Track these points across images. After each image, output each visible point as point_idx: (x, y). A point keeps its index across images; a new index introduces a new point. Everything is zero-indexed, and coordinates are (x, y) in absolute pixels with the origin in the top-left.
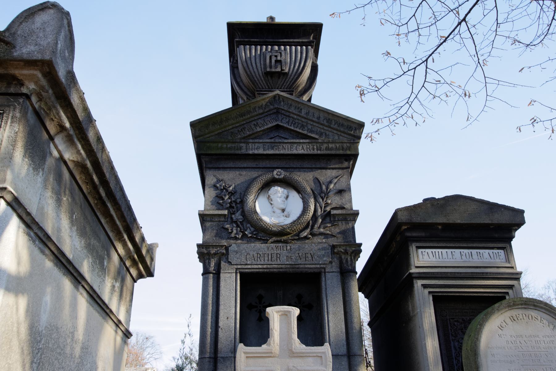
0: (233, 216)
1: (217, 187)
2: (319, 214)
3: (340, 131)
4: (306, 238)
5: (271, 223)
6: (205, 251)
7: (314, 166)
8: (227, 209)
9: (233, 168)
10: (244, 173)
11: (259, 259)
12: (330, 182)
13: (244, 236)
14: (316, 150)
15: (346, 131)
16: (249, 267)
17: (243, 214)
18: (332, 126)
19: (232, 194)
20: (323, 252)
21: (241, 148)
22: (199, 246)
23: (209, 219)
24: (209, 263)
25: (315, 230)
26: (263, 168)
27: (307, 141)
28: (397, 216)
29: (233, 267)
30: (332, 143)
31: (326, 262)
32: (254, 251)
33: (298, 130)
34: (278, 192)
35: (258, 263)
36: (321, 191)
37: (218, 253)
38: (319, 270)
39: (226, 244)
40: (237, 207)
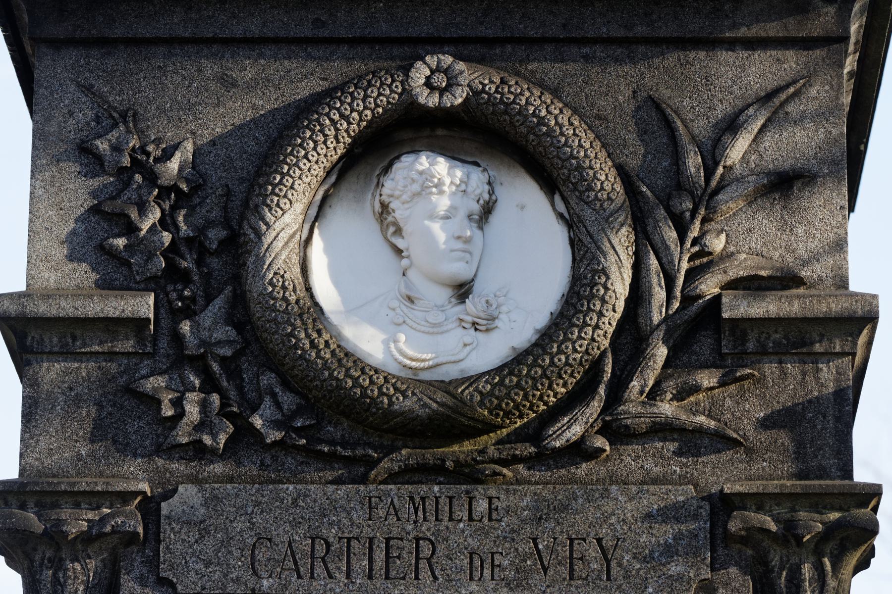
0: (186, 327)
1: (99, 158)
2: (656, 318)
4: (579, 451)
5: (393, 369)
7: (641, 30)
8: (149, 284)
9: (183, 41)
10: (248, 70)
11: (319, 570)
12: (732, 126)
13: (245, 437)
17: (241, 314)
19: (177, 197)
20: (666, 532)
23: (52, 340)
26: (353, 42)
32: (295, 524)
34: (435, 179)
36: (678, 182)
37: (101, 535)
39: (145, 487)
40: (207, 278)
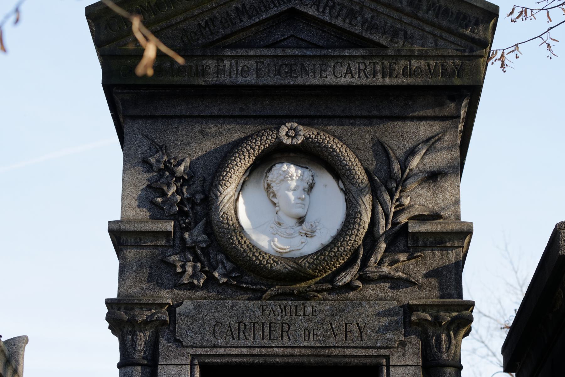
0: (187, 235)
1: (151, 165)
2: (381, 232)
3: (440, 27)
4: (349, 287)
5: (272, 252)
6: (123, 315)
7: (375, 113)
9: (186, 117)
11: (242, 336)
13: (211, 281)
14: (379, 76)
15: (453, 27)
16: (221, 351)
18: (420, 14)
19: (183, 181)
20: (385, 321)
21: (204, 73)
22: (109, 303)
23: (132, 241)
24: (134, 342)
25: (371, 269)
26: (255, 117)
27: (361, 52)
28: (559, 239)
29: (185, 351)
30: (419, 57)
31: (391, 344)
32: (232, 317)
33: (339, 22)
34: (290, 175)
35: (241, 343)
36: (390, 176)
37: (152, 321)
38: (374, 361)
39: (170, 301)
40: (195, 215)
